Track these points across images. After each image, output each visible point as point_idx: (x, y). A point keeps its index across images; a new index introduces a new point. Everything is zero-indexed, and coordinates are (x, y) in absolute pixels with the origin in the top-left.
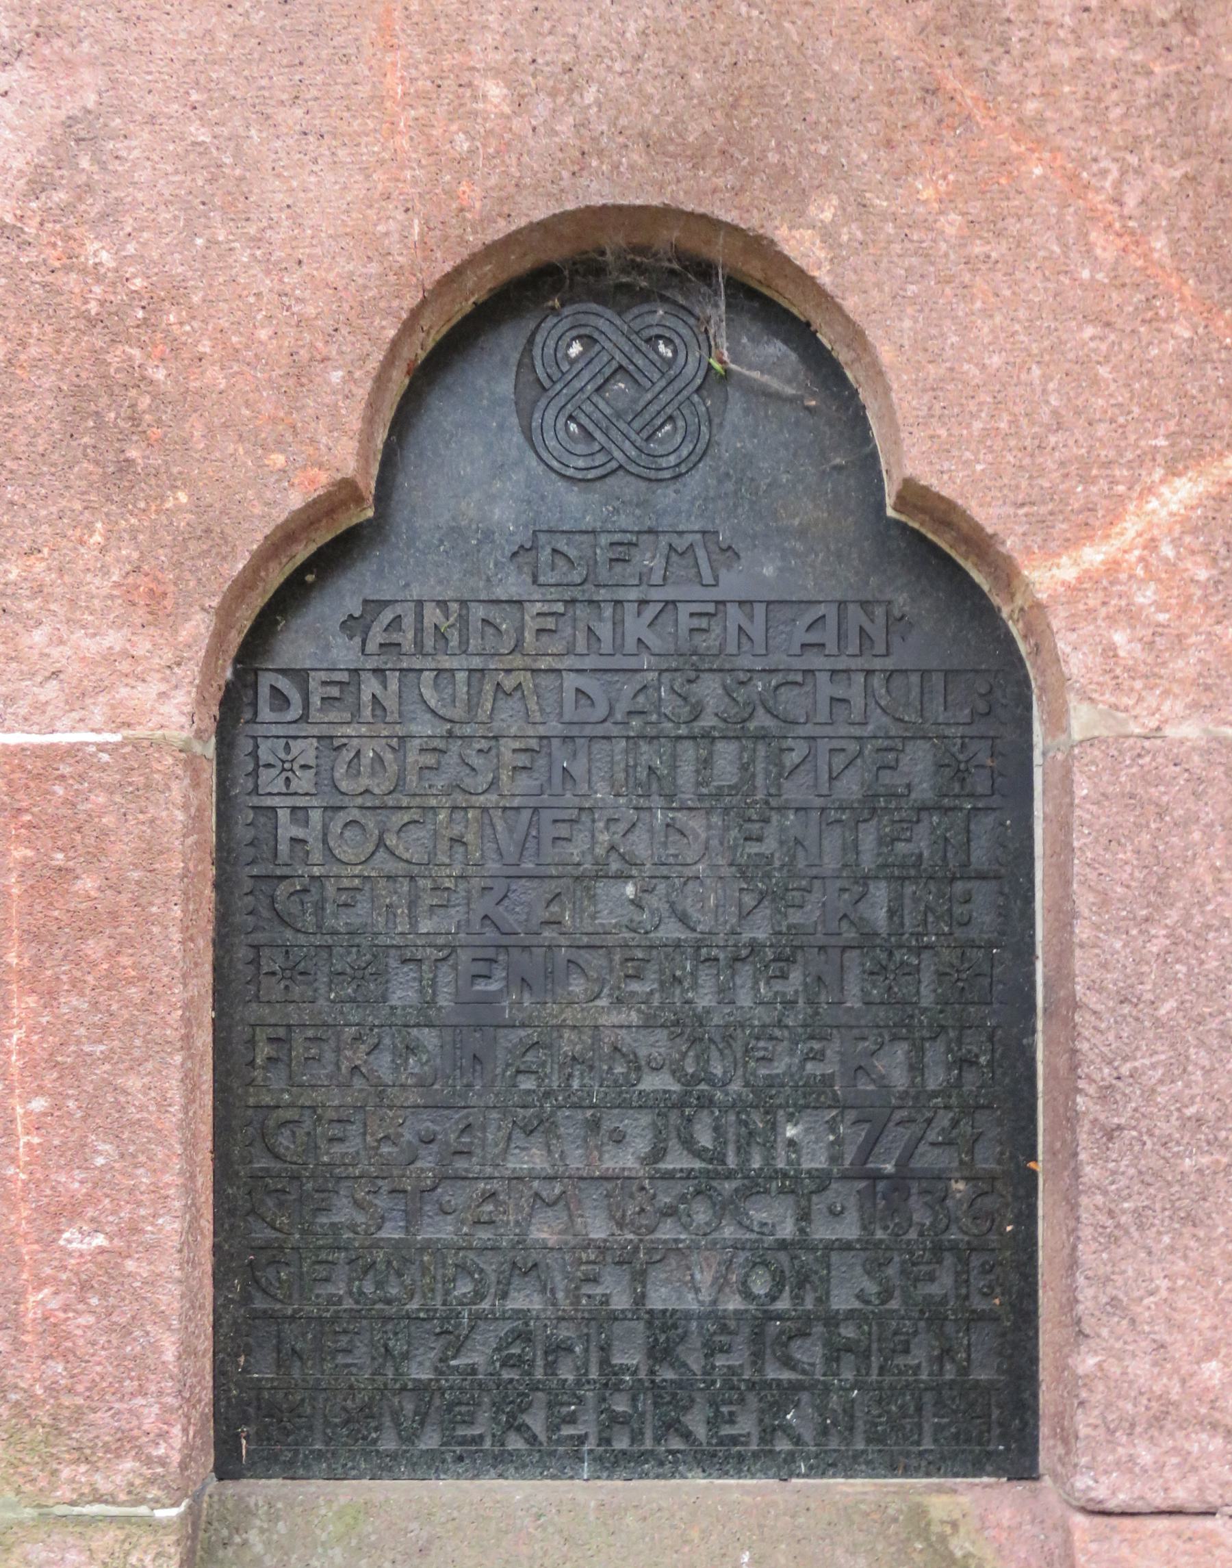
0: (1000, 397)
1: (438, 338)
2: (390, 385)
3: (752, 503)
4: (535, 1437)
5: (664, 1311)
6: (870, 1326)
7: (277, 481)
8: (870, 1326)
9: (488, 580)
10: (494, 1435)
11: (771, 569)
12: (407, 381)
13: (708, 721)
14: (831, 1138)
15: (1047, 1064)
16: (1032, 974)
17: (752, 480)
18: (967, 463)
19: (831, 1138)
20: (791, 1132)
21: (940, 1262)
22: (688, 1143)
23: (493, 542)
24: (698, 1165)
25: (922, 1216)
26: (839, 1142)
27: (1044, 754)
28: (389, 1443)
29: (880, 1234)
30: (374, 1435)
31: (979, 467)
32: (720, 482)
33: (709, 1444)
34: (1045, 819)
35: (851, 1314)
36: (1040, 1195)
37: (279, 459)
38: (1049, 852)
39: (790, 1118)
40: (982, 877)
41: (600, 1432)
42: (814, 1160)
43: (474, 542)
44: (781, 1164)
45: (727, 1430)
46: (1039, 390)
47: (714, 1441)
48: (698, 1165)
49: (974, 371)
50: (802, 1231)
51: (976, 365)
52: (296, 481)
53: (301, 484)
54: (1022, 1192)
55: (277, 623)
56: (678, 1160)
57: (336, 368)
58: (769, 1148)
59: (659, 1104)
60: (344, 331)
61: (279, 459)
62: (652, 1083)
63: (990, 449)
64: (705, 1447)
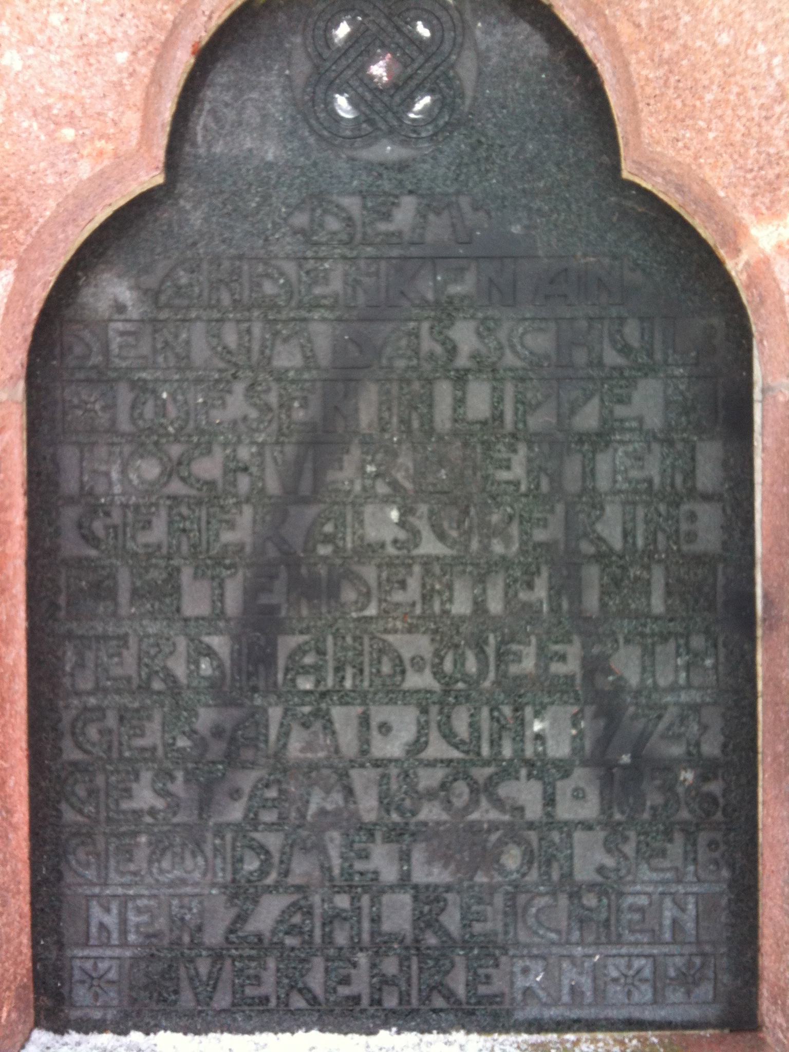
0: (729, 71)
1: (220, 21)
2: (176, 64)
3: (502, 168)
4: (315, 998)
5: (427, 887)
6: (609, 899)
7: (68, 153)
8: (609, 899)
9: (266, 240)
10: (278, 998)
11: (519, 227)
12: (192, 61)
13: (462, 361)
14: (574, 732)
15: (767, 668)
16: (752, 581)
17: (502, 147)
18: (700, 131)
19: (574, 732)
20: (537, 726)
21: (671, 841)
22: (449, 736)
23: (270, 205)
24: (456, 754)
25: (654, 798)
26: (581, 735)
27: (763, 391)
28: (187, 999)
29: (618, 817)
30: (173, 997)
31: (711, 135)
32: (474, 149)
33: (468, 1003)
34: (764, 449)
35: (592, 886)
36: (760, 783)
37: (69, 134)
38: (768, 480)
39: (537, 714)
40: (707, 498)
41: (372, 993)
42: (559, 749)
43: (254, 205)
44: (529, 753)
45: (482, 990)
46: (764, 66)
47: (473, 1001)
48: (456, 754)
49: (706, 47)
50: (549, 815)
51: (708, 41)
52: (85, 152)
53: (89, 155)
54: (743, 780)
55: (78, 278)
56: (437, 748)
57: (122, 49)
58: (519, 738)
59: (422, 701)
60: (129, 15)
61: (69, 134)
62: (415, 680)
63: (721, 118)
64: (465, 1006)
